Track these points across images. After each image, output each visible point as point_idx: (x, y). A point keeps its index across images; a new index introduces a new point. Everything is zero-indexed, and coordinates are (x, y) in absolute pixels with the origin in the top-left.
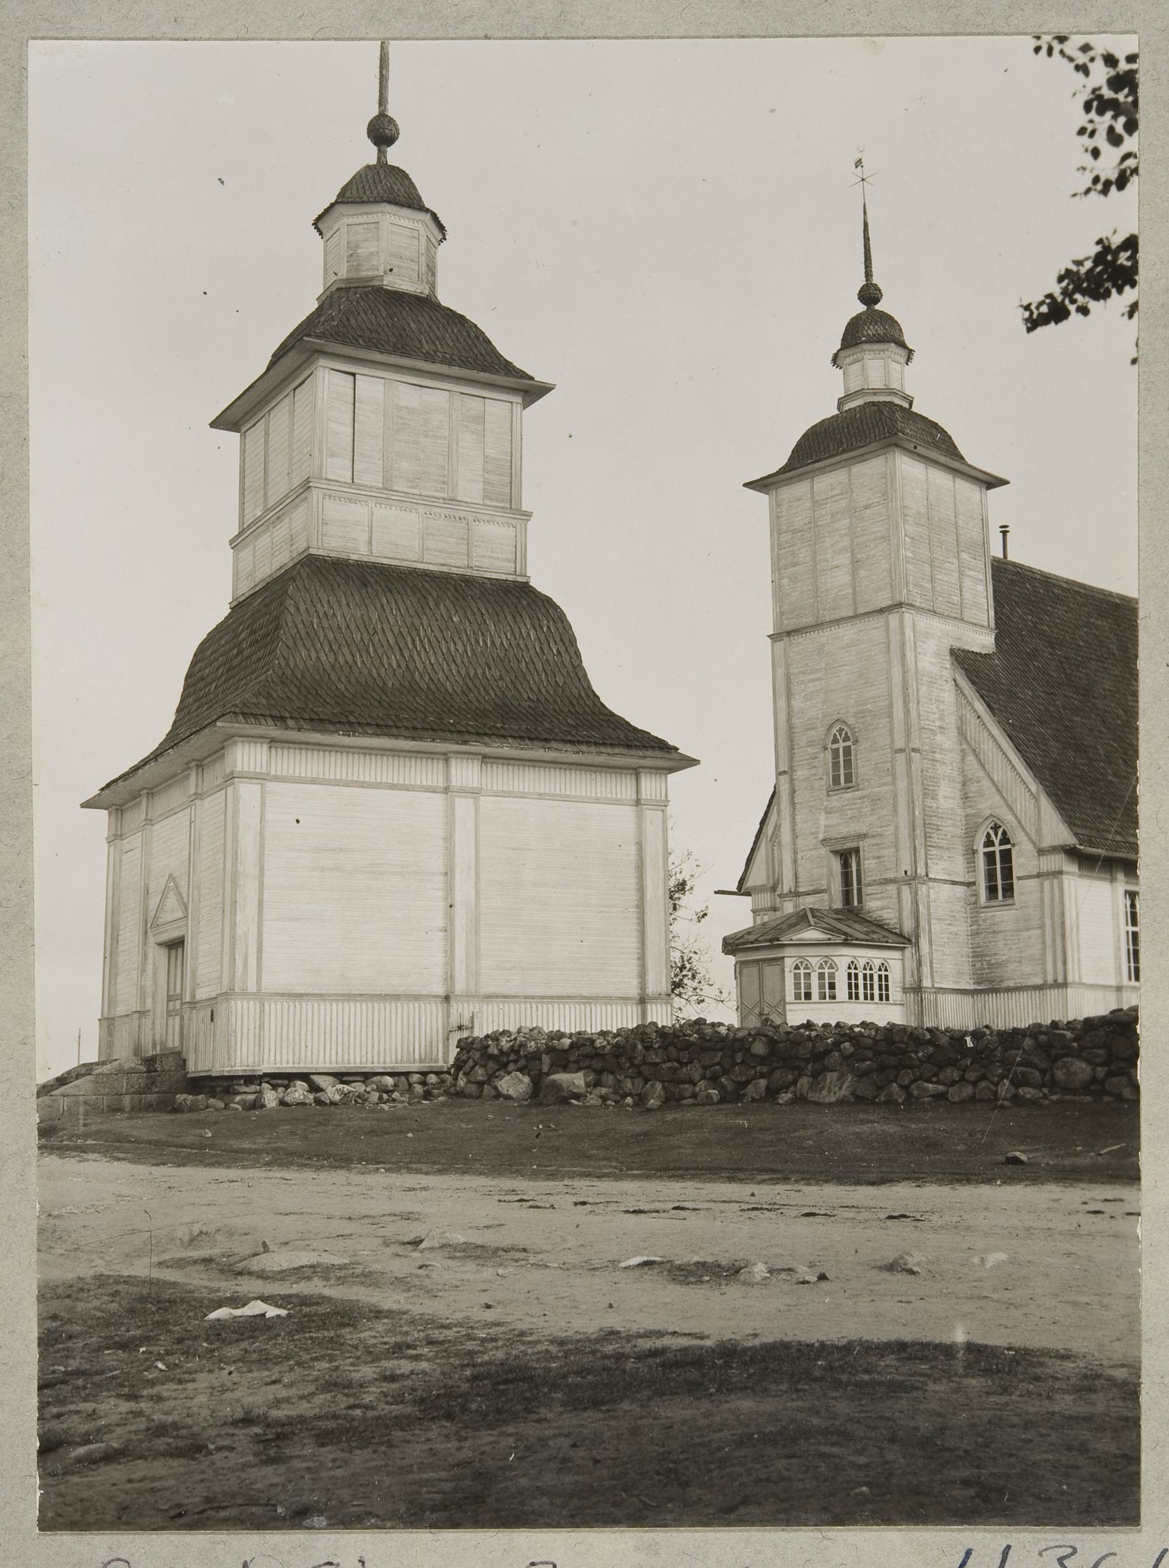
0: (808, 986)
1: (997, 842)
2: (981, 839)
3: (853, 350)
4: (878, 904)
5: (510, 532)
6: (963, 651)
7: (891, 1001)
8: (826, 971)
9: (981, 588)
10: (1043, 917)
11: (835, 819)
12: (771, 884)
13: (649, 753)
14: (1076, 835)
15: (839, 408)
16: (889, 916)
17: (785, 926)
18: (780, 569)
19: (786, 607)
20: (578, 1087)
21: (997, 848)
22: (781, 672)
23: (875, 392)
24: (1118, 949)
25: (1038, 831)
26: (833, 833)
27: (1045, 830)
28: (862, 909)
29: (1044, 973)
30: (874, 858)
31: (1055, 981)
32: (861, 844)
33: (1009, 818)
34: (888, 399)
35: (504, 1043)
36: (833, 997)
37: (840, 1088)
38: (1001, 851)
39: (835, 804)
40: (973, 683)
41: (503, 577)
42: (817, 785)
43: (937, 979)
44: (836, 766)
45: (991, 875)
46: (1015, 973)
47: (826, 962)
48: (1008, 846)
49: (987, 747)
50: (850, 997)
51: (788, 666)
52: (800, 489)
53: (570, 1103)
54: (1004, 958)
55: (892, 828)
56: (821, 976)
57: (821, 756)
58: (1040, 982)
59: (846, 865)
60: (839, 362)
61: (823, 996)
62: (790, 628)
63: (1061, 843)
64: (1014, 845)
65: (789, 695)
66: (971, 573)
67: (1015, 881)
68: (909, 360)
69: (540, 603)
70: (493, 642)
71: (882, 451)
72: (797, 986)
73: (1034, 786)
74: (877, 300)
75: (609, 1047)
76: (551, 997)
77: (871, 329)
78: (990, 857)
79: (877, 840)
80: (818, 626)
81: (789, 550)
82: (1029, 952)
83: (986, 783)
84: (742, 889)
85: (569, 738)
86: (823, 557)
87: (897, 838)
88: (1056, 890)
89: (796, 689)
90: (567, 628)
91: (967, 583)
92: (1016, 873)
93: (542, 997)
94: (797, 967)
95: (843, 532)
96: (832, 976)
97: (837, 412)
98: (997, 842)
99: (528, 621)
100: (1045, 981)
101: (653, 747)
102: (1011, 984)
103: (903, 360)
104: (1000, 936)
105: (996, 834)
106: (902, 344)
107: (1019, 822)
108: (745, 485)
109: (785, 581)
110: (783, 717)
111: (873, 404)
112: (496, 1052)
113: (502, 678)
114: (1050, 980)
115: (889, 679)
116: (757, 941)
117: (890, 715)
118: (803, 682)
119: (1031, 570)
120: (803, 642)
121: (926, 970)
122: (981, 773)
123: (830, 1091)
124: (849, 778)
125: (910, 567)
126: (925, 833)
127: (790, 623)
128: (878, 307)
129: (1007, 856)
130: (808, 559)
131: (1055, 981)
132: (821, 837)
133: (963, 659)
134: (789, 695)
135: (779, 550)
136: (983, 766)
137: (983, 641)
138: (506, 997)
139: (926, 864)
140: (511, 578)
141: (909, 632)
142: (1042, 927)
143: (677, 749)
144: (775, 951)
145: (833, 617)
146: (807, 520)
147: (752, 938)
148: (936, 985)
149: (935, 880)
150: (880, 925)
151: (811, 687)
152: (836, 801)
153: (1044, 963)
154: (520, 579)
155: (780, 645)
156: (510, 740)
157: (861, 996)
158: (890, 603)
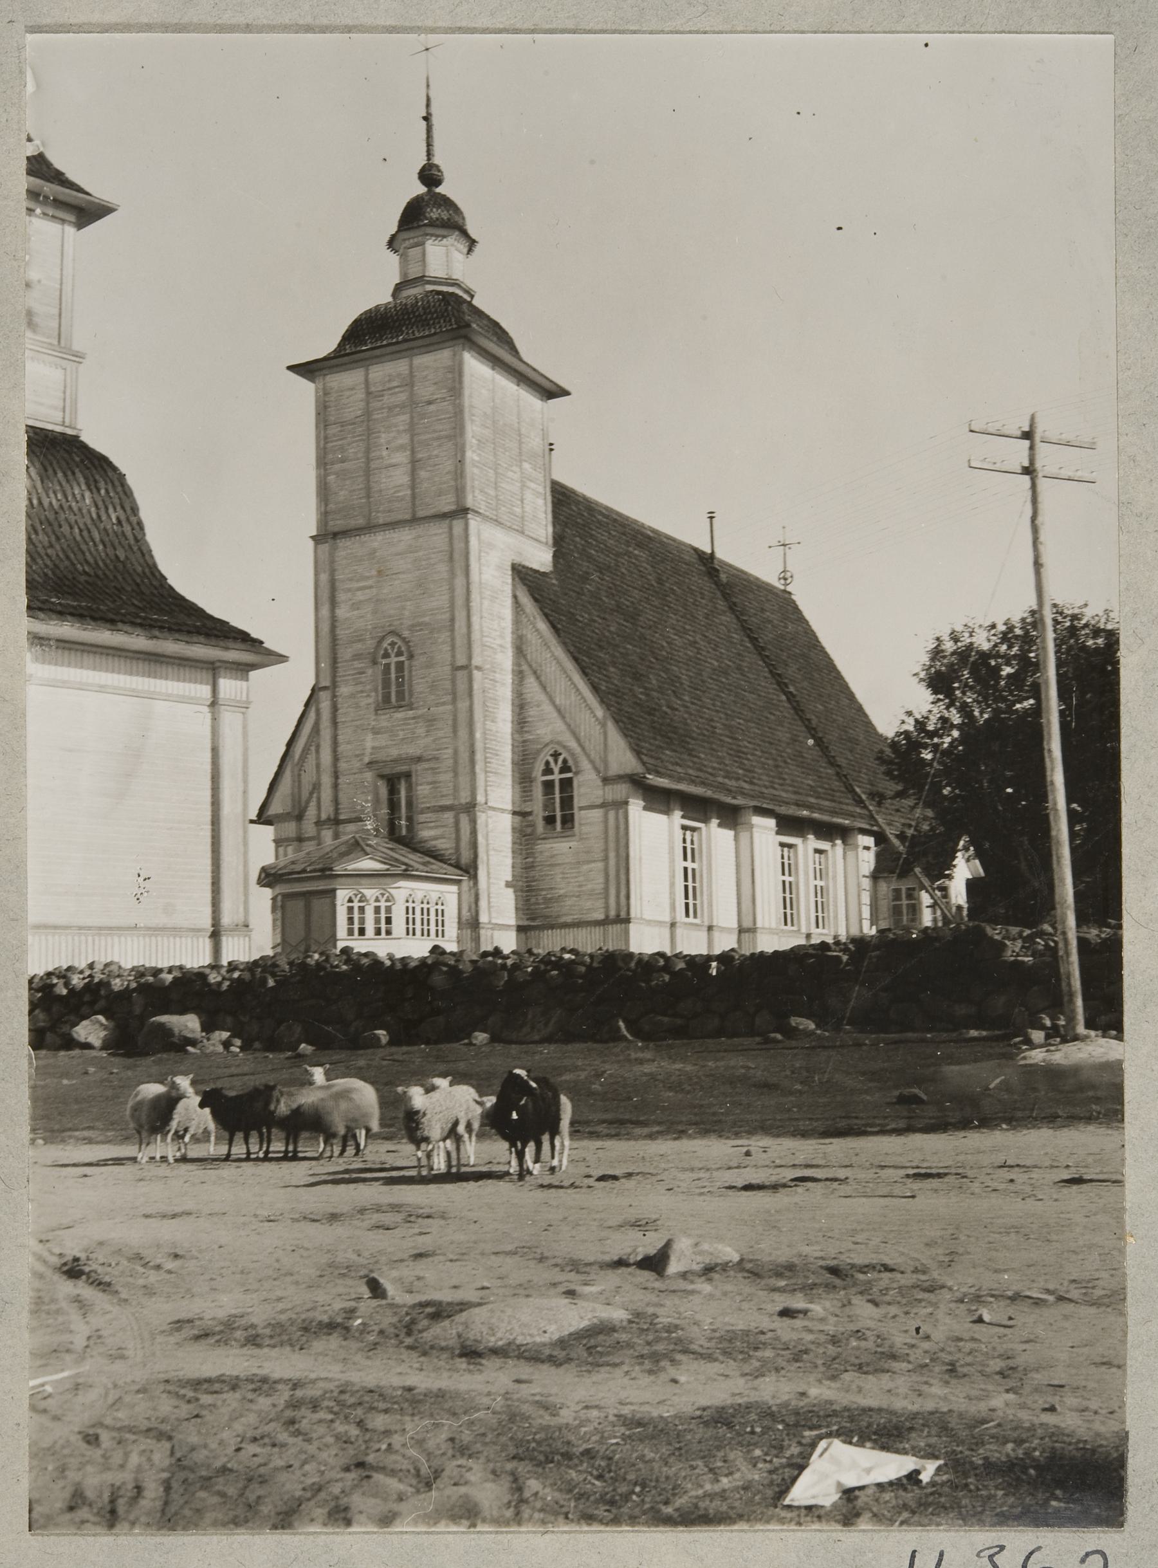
0: (362, 921)
1: (556, 770)
2: (540, 767)
3: (411, 234)
4: (432, 833)
5: (58, 374)
6: (524, 567)
7: (446, 938)
8: (383, 904)
9: (540, 502)
10: (606, 850)
11: (383, 740)
12: (296, 813)
13: (231, 644)
14: (644, 763)
15: (394, 295)
16: (444, 846)
17: (335, 855)
18: (326, 464)
19: (332, 506)
20: (193, 1031)
21: (556, 777)
22: (324, 577)
23: (437, 281)
24: (672, 885)
25: (605, 761)
26: (381, 756)
27: (612, 758)
28: (412, 838)
29: (607, 907)
30: (429, 783)
31: (618, 916)
32: (414, 767)
33: (573, 744)
34: (451, 289)
35: (76, 981)
36: (388, 932)
37: (546, 1025)
38: (561, 780)
39: (385, 724)
40: (536, 600)
41: (50, 427)
42: (364, 702)
43: (494, 915)
44: (386, 683)
45: (548, 805)
46: (569, 910)
47: (383, 895)
48: (569, 775)
49: (551, 670)
50: (408, 934)
51: (333, 572)
52: (349, 379)
53: (186, 1052)
54: (562, 892)
55: (450, 751)
56: (377, 910)
57: (370, 671)
58: (601, 917)
59: (393, 791)
60: (396, 244)
61: (378, 932)
62: (336, 529)
63: (628, 771)
64: (577, 773)
65: (333, 603)
66: (532, 485)
67: (576, 811)
68: (470, 251)
69: (97, 463)
70: (40, 503)
71: (451, 343)
72: (351, 920)
73: (600, 713)
74: (438, 182)
75: (227, 983)
76: (110, 928)
77: (428, 213)
78: (548, 786)
79: (432, 765)
80: (370, 528)
81: (339, 445)
82: (589, 887)
83: (548, 708)
84: (263, 818)
85: (139, 621)
86: (378, 453)
87: (456, 762)
88: (622, 820)
89: (341, 597)
90: (127, 493)
91: (529, 496)
92: (577, 803)
93: (100, 928)
94: (350, 900)
95: (401, 428)
96: (388, 910)
97: (391, 299)
98: (556, 770)
99: (82, 480)
100: (607, 917)
101: (235, 639)
102: (569, 919)
103: (465, 250)
104: (558, 870)
105: (556, 762)
106: (464, 233)
107: (583, 749)
108: (290, 368)
109: (331, 478)
110: (325, 628)
111: (439, 293)
112: (65, 992)
113: (51, 546)
114: (612, 913)
115: (452, 590)
116: (304, 871)
117: (452, 630)
118: (349, 590)
119: (573, 492)
120: (347, 547)
121: (483, 904)
122: (542, 697)
123: (533, 1028)
124: (400, 695)
125: (476, 471)
126: (486, 758)
127: (337, 524)
128: (438, 190)
129: (567, 784)
130: (360, 455)
131: (618, 916)
132: (367, 760)
133: (522, 574)
134: (333, 603)
135: (326, 443)
136: (544, 688)
137: (541, 558)
138: (56, 927)
139: (486, 791)
140: (58, 429)
141: (473, 541)
142: (606, 859)
143: (262, 642)
144: (327, 881)
145: (388, 520)
146: (359, 413)
147: (298, 868)
148: (494, 921)
149: (494, 809)
150: (435, 855)
151: (360, 596)
152: (384, 721)
153: (607, 898)
154: (69, 432)
155: (325, 548)
156: (69, 618)
157: (418, 932)
158: (453, 507)
